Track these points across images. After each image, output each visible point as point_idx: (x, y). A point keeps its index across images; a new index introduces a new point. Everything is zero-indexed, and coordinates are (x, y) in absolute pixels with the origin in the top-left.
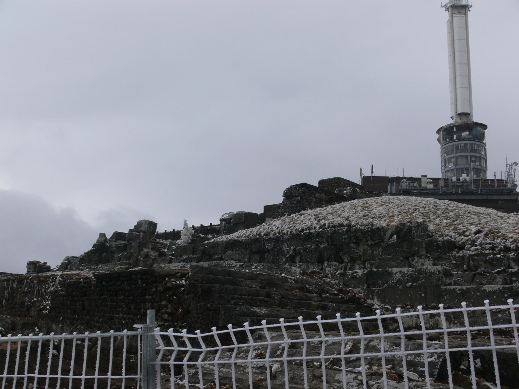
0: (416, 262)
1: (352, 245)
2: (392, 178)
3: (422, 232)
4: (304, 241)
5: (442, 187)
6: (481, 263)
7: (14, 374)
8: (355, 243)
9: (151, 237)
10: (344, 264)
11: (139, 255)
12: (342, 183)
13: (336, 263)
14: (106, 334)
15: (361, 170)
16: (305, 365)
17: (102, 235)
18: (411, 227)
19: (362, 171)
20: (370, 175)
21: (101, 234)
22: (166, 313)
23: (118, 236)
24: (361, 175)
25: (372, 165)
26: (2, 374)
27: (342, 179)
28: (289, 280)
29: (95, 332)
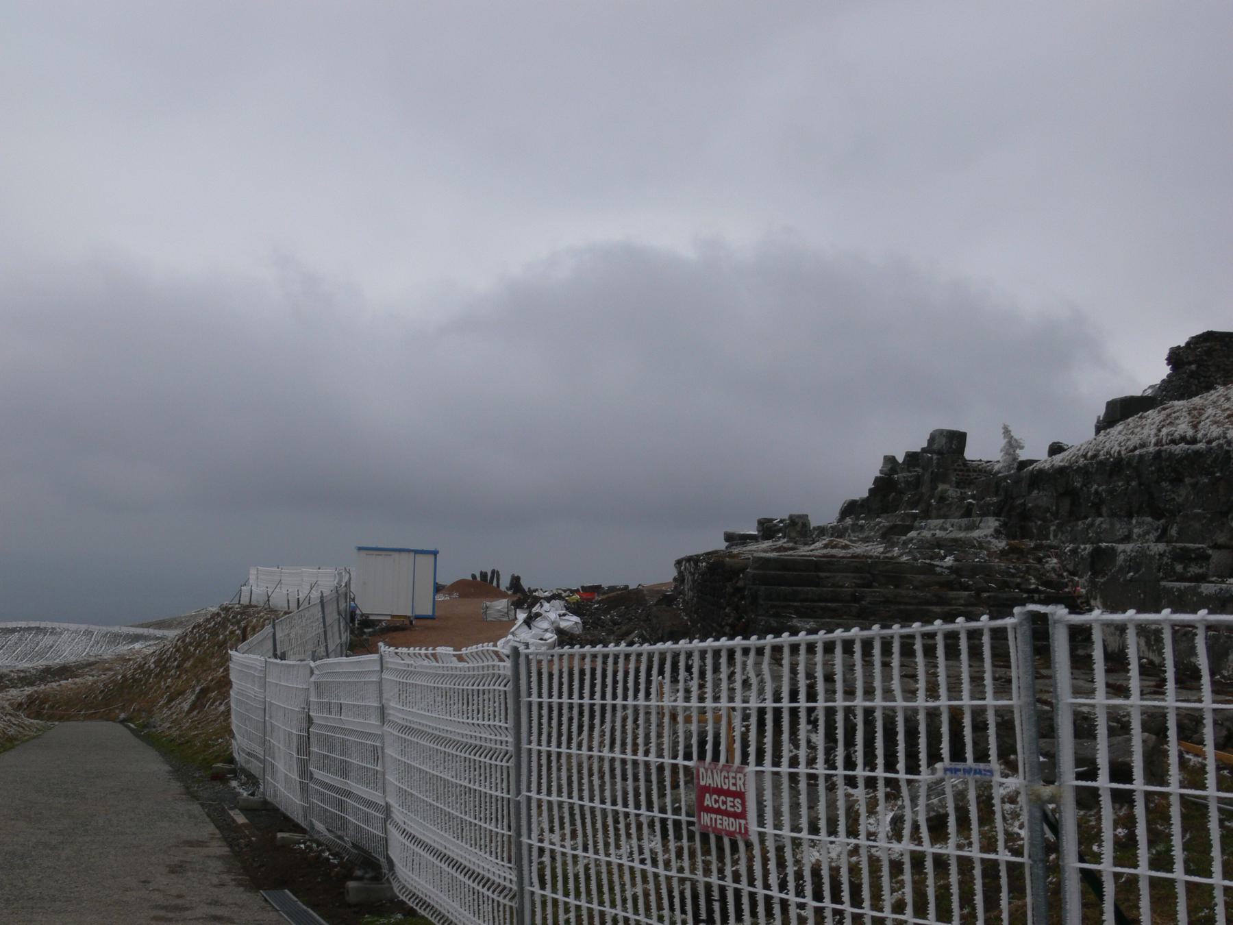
1: (1164, 484)
10: (1162, 521)
13: (1149, 519)
17: (890, 460)
18: (1228, 451)
21: (885, 457)
23: (912, 457)
28: (938, 569)
29: (930, 622)
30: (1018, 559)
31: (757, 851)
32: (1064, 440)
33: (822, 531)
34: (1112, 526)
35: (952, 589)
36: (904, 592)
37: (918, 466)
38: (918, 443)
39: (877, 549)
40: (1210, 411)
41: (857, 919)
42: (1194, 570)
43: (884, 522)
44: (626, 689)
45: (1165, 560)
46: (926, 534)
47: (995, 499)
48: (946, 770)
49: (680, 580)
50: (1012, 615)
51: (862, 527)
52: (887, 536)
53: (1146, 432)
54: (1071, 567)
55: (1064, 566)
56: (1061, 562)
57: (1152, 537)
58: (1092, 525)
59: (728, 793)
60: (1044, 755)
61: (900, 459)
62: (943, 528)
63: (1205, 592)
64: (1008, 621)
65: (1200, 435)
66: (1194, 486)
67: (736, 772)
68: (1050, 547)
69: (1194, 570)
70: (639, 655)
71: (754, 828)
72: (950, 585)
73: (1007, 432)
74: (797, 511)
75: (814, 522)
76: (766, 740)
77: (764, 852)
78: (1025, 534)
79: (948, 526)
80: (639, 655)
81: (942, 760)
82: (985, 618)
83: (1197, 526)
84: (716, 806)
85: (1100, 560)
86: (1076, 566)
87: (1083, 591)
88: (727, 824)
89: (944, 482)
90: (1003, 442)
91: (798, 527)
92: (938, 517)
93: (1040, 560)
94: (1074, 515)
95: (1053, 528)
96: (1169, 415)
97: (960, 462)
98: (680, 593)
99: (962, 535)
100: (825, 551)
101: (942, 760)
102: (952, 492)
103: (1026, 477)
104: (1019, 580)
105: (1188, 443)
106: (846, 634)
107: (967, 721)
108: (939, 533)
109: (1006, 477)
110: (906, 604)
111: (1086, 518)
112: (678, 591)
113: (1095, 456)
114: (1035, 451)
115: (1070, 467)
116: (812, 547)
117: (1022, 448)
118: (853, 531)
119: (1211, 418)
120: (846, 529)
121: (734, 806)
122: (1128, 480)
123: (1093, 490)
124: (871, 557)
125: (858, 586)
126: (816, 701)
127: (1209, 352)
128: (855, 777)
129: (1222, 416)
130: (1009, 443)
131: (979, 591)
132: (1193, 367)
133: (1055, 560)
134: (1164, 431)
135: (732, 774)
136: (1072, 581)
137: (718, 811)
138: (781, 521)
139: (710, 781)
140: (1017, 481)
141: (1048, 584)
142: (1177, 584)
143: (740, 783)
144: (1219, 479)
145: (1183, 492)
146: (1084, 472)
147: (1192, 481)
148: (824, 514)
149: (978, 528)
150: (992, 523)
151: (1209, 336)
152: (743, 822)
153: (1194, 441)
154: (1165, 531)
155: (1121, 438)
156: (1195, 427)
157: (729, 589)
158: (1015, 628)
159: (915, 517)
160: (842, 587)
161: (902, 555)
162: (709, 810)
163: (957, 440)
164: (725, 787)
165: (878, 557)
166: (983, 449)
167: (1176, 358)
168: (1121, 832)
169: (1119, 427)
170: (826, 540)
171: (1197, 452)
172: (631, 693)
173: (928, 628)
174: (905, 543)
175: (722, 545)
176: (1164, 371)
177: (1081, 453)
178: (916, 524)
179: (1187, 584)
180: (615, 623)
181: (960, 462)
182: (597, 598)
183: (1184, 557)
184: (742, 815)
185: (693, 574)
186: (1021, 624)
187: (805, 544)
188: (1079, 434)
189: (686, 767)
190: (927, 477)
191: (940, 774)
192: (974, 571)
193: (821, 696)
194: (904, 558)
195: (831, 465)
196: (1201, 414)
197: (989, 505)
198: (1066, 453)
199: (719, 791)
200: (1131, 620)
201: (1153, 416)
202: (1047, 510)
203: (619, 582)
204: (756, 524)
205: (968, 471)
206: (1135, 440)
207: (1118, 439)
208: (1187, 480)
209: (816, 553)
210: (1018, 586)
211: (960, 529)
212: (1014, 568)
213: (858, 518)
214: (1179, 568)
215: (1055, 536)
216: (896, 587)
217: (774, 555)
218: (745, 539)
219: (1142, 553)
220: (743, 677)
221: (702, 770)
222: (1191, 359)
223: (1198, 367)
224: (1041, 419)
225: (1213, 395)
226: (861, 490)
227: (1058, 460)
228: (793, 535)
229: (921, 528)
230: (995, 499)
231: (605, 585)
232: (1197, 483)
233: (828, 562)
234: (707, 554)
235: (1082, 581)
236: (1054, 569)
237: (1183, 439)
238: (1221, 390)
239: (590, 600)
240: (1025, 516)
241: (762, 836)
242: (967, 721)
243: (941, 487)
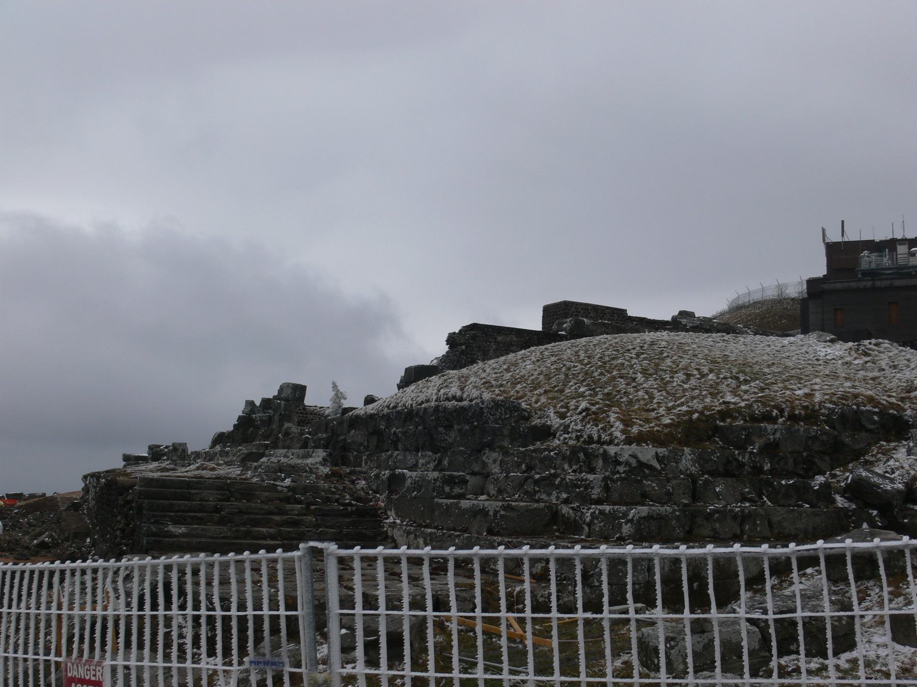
0: (488, 457)
1: (440, 429)
2: (881, 242)
3: (506, 414)
4: (405, 421)
6: (537, 462)
9: (297, 407)
11: (279, 432)
12: (573, 310)
13: (430, 453)
14: (224, 558)
15: (824, 230)
17: (250, 404)
19: (827, 233)
20: (840, 240)
23: (266, 402)
24: (824, 240)
25: (843, 222)
26: (2, 607)
27: (573, 303)
30: (338, 481)
33: (197, 455)
34: (405, 457)
35: (289, 503)
36: (253, 505)
37: (270, 408)
39: (235, 472)
40: (472, 379)
41: (296, 679)
42: (457, 490)
43: (244, 449)
44: (11, 600)
46: (274, 459)
47: (324, 435)
48: (251, 662)
49: (86, 490)
50: (299, 549)
51: (227, 453)
52: (246, 460)
53: (430, 391)
54: (374, 487)
55: (370, 487)
56: (368, 484)
57: (431, 466)
58: (391, 456)
60: (347, 629)
61: (258, 403)
62: (286, 456)
63: (464, 507)
64: (296, 554)
65: (465, 396)
66: (460, 430)
67: (96, 666)
68: (361, 472)
69: (457, 490)
70: (23, 572)
72: (287, 500)
73: (335, 386)
74: (179, 440)
75: (191, 449)
78: (345, 462)
79: (290, 454)
80: (23, 572)
81: (248, 655)
83: (461, 459)
85: (395, 481)
86: (378, 486)
89: (289, 422)
90: (332, 394)
91: (178, 453)
92: (284, 448)
93: (353, 482)
94: (380, 448)
95: (364, 457)
96: (445, 380)
97: (301, 407)
98: (85, 501)
99: (299, 461)
100: (196, 473)
101: (248, 655)
102: (295, 429)
103: (348, 420)
106: (181, 559)
107: (266, 626)
108: (283, 460)
109: (333, 420)
111: (387, 451)
112: (84, 500)
113: (395, 407)
114: (354, 401)
115: (378, 414)
116: (188, 468)
117: (345, 399)
118: (221, 456)
120: (215, 454)
123: (392, 431)
124: (230, 478)
125: (220, 500)
126: (157, 610)
127: (474, 337)
129: (480, 383)
130: (336, 394)
131: (309, 504)
132: (463, 347)
133: (364, 482)
134: (442, 391)
135: (92, 667)
136: (375, 497)
138: (166, 447)
139: (75, 673)
140: (341, 423)
141: (359, 499)
143: (98, 674)
144: (476, 427)
145: (453, 434)
146: (387, 418)
148: (199, 442)
149: (311, 457)
150: (320, 454)
151: (474, 327)
153: (461, 399)
154: (440, 461)
155: (413, 395)
156: (462, 389)
157: (121, 502)
158: (300, 558)
159: (266, 446)
160: (208, 501)
161: (253, 477)
163: (299, 391)
164: (87, 678)
165: (235, 479)
167: (452, 340)
168: (440, 638)
169: (412, 387)
170: (200, 462)
171: (462, 408)
172: (14, 603)
173: (239, 557)
174: (256, 468)
175: (119, 464)
176: (442, 349)
178: (267, 452)
180: (30, 525)
181: (301, 407)
182: (18, 504)
183: (450, 481)
185: (95, 487)
186: (304, 556)
187: (183, 466)
188: (387, 390)
189: (56, 662)
190: (276, 417)
191: (246, 666)
192: (305, 489)
193: (161, 607)
194: (255, 480)
195: (207, 401)
196: (466, 381)
197: (320, 439)
198: (376, 404)
200: (380, 554)
201: (435, 380)
202: (361, 444)
203: (39, 492)
204: (147, 449)
205: (307, 414)
206: (422, 397)
207: (412, 395)
208: (456, 427)
209: (189, 474)
210: (337, 501)
211: (298, 457)
213: (225, 446)
214: (447, 489)
215: (366, 463)
216: (248, 501)
217: (156, 475)
218: (138, 460)
219: (423, 478)
220: (106, 587)
221: (69, 664)
222: (462, 341)
223: (466, 348)
224: (358, 377)
225: (475, 368)
226: (228, 425)
227: (371, 409)
228: (174, 458)
229: (271, 455)
230: (324, 435)
231: (26, 493)
232: (461, 429)
233: (198, 482)
234: (107, 472)
236: (362, 488)
238: (480, 364)
239: (12, 506)
240: (345, 448)
242: (266, 626)
243: (287, 425)
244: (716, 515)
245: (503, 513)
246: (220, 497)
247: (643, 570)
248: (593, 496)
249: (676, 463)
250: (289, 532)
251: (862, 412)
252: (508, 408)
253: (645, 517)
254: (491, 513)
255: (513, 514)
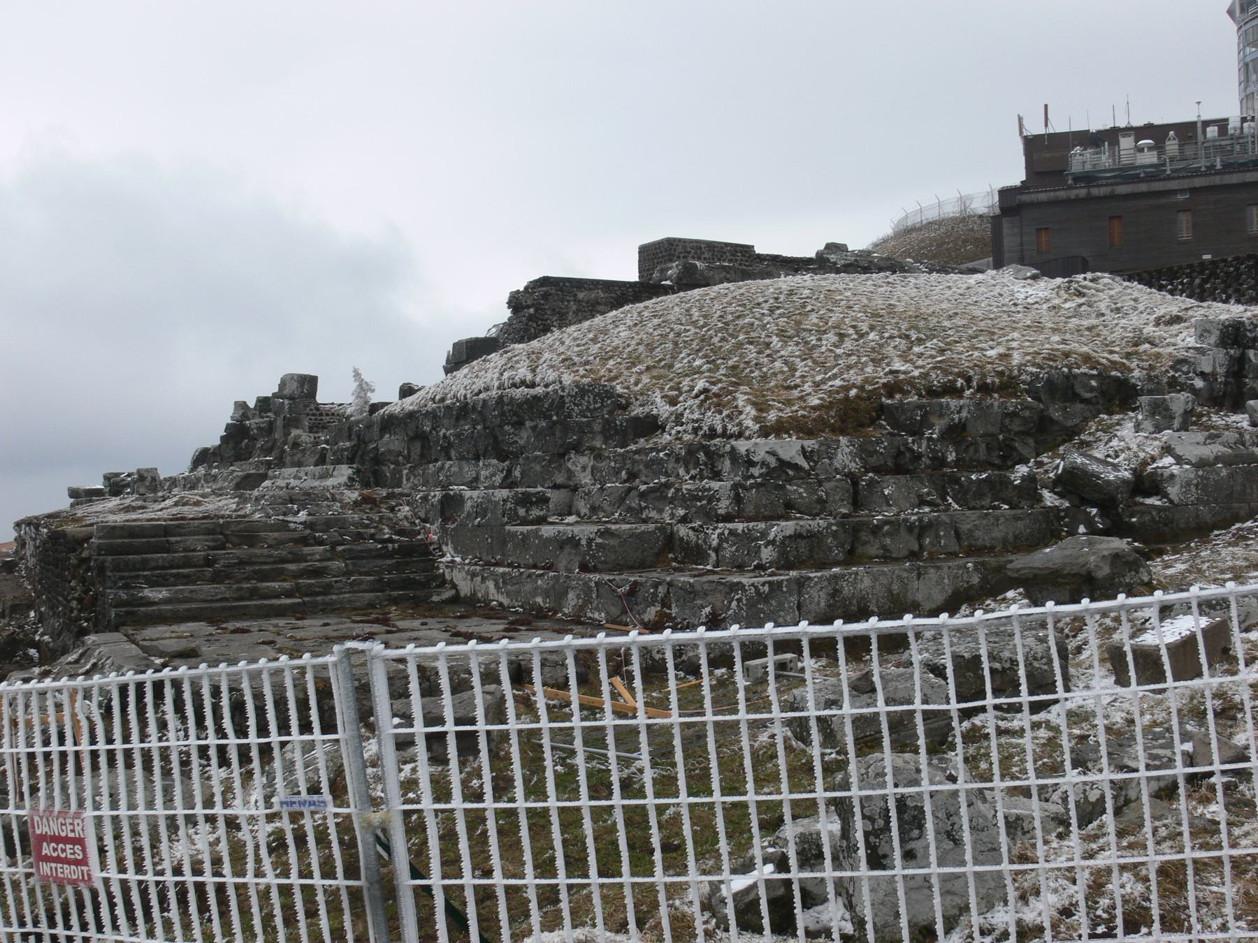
1: (506, 428)
2: (1099, 132)
3: (596, 403)
4: (457, 419)
5: (1172, 159)
7: (984, 698)
8: (513, 425)
11: (285, 443)
13: (495, 461)
15: (1020, 119)
16: (841, 647)
17: (241, 406)
18: (562, 397)
19: (1025, 122)
22: (74, 598)
23: (264, 403)
25: (1046, 106)
27: (680, 240)
28: (291, 525)
30: (371, 509)
31: (103, 898)
32: (416, 382)
33: (173, 482)
34: (461, 469)
36: (258, 551)
38: (269, 388)
40: (546, 355)
42: (536, 512)
43: (238, 470)
45: (509, 505)
46: (281, 483)
49: (21, 542)
50: (332, 653)
51: (215, 477)
53: (489, 375)
54: (422, 514)
55: (415, 514)
58: (442, 468)
59: (66, 840)
61: (252, 404)
63: (546, 535)
64: (329, 659)
65: (538, 380)
66: (534, 428)
68: (402, 495)
69: (536, 512)
71: (98, 875)
72: (304, 541)
73: (357, 375)
75: (163, 475)
76: (101, 784)
77: (110, 897)
78: (379, 481)
82: (307, 656)
83: (538, 468)
84: (55, 855)
85: (450, 504)
86: (427, 513)
87: (435, 538)
88: (69, 871)
90: (354, 385)
92: (294, 465)
93: (392, 509)
94: (425, 458)
95: (405, 472)
96: (510, 359)
98: (22, 559)
99: (316, 483)
102: (306, 438)
103: (382, 421)
104: (373, 531)
105: (527, 387)
109: (358, 422)
110: (261, 563)
111: (436, 460)
113: (443, 400)
114: (386, 393)
117: (373, 391)
118: (207, 482)
119: (548, 363)
120: (198, 480)
121: (74, 853)
122: (475, 423)
123: (441, 433)
124: (223, 517)
125: (210, 548)
127: (545, 296)
128: (194, 815)
130: (360, 386)
132: (532, 311)
133: (407, 508)
134: (506, 375)
136: (424, 528)
137: (58, 860)
138: (129, 475)
139: (46, 829)
140: (369, 427)
141: (401, 532)
142: (520, 528)
143: (78, 829)
144: (555, 423)
145: (524, 434)
146: (432, 415)
147: (532, 424)
148: (174, 464)
149: (332, 476)
150: (344, 472)
152: (85, 868)
153: (533, 385)
155: (467, 382)
156: (533, 371)
157: (74, 561)
158: (335, 665)
159: (269, 464)
160: (194, 550)
161: (255, 511)
162: (48, 859)
163: (309, 384)
164: (63, 834)
165: (230, 516)
166: (334, 392)
167: (516, 302)
171: (535, 397)
176: (505, 314)
177: (429, 396)
179: (529, 528)
183: (526, 501)
184: (84, 862)
185: (34, 540)
186: (340, 661)
188: (430, 375)
190: (279, 423)
192: (328, 524)
194: (257, 516)
196: (538, 358)
197: (343, 450)
199: (57, 839)
201: (496, 359)
202: (400, 453)
205: (321, 415)
206: (479, 384)
207: (467, 382)
208: (528, 424)
210: (372, 536)
212: (368, 519)
213: (210, 467)
214: (522, 512)
221: (36, 818)
223: (536, 311)
225: (549, 338)
226: (213, 438)
227: (410, 403)
228: (142, 490)
229: (275, 477)
232: (536, 427)
233: (178, 526)
234: (50, 516)
235: (434, 527)
236: (406, 517)
237: (523, 383)
240: (378, 460)
241: (106, 881)
243: (294, 432)
244: (886, 528)
245: (599, 540)
246: (210, 544)
247: (790, 607)
248: (720, 511)
249: (830, 459)
250: (310, 585)
251: (1076, 376)
252: (598, 394)
253: (790, 536)
254: (584, 542)
255: (613, 542)
